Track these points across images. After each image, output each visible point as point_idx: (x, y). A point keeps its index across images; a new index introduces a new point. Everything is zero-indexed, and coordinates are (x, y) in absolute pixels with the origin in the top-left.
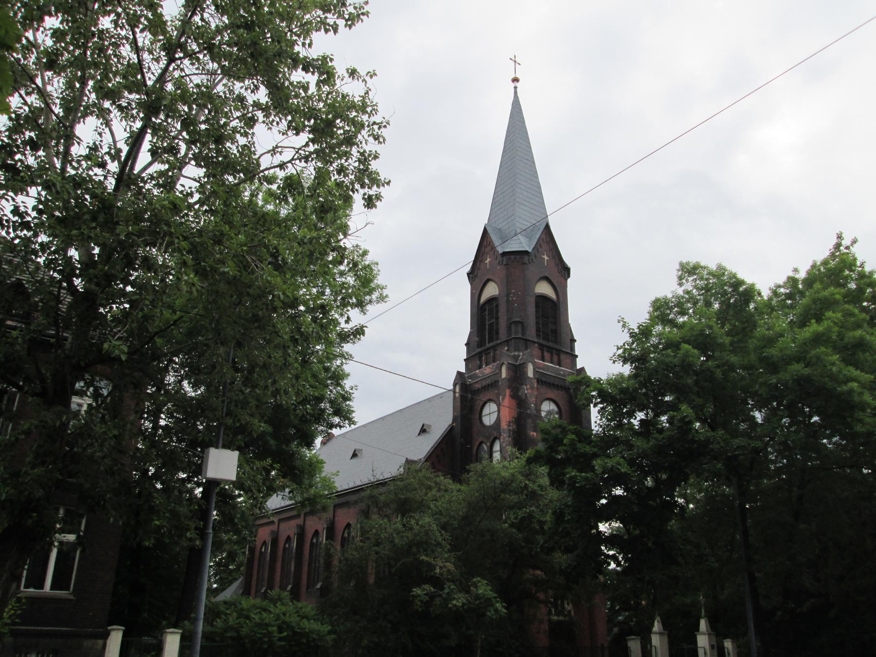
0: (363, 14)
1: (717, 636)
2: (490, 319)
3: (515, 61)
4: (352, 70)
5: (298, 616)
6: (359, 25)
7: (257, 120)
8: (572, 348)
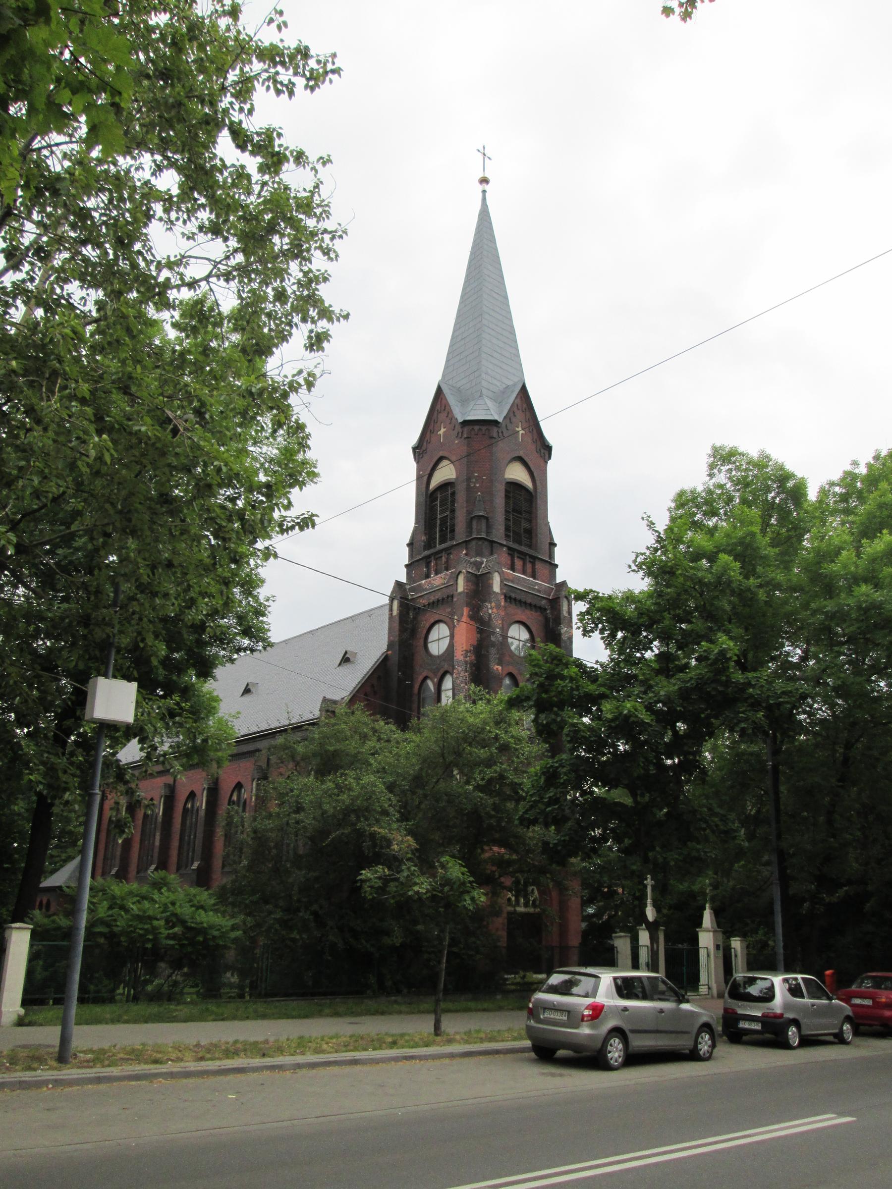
0: (333, 72)
1: (724, 933)
2: (442, 512)
3: (484, 154)
4: (298, 152)
5: (192, 906)
6: (325, 87)
7: (153, 216)
8: (551, 555)
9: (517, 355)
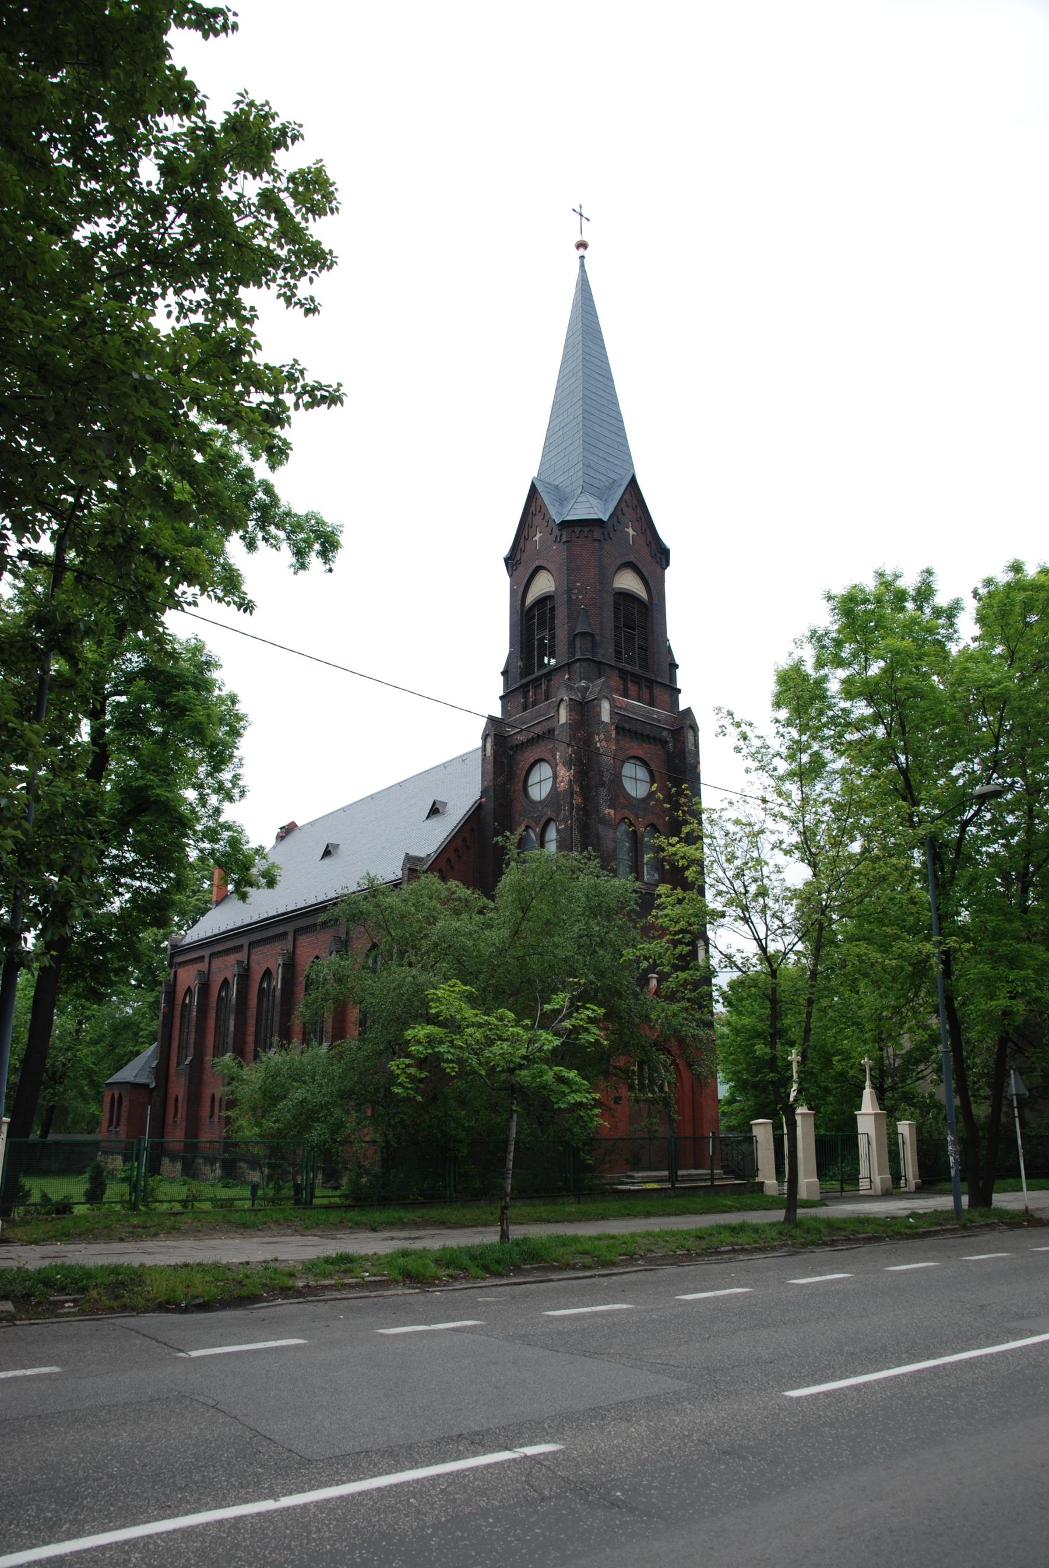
3: (581, 215)
8: (673, 678)
9: (626, 445)
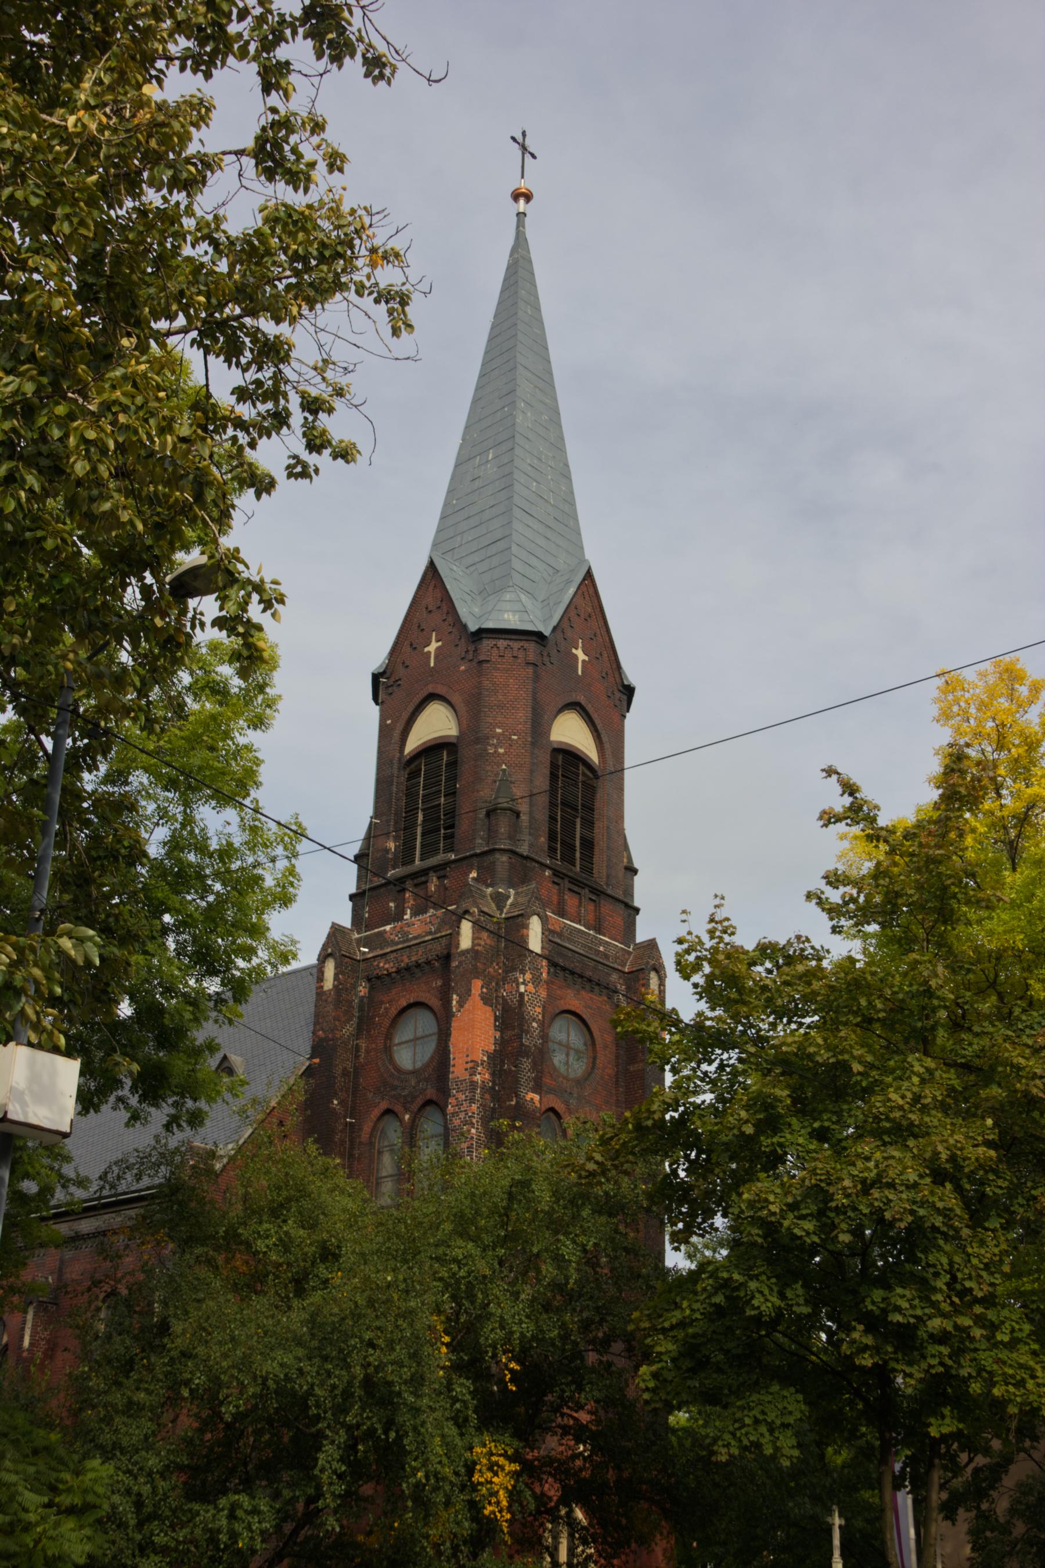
8: (629, 891)
